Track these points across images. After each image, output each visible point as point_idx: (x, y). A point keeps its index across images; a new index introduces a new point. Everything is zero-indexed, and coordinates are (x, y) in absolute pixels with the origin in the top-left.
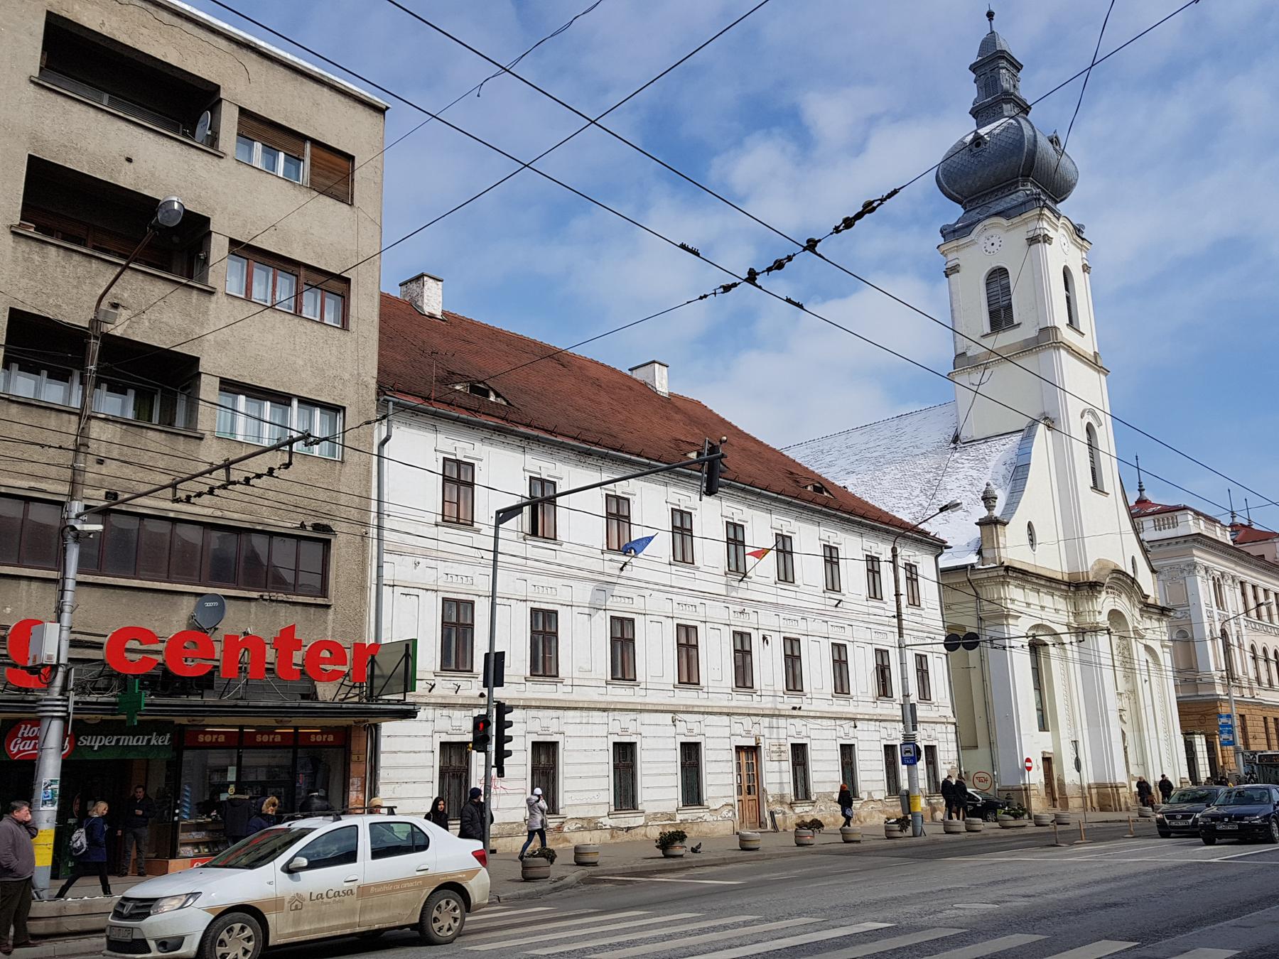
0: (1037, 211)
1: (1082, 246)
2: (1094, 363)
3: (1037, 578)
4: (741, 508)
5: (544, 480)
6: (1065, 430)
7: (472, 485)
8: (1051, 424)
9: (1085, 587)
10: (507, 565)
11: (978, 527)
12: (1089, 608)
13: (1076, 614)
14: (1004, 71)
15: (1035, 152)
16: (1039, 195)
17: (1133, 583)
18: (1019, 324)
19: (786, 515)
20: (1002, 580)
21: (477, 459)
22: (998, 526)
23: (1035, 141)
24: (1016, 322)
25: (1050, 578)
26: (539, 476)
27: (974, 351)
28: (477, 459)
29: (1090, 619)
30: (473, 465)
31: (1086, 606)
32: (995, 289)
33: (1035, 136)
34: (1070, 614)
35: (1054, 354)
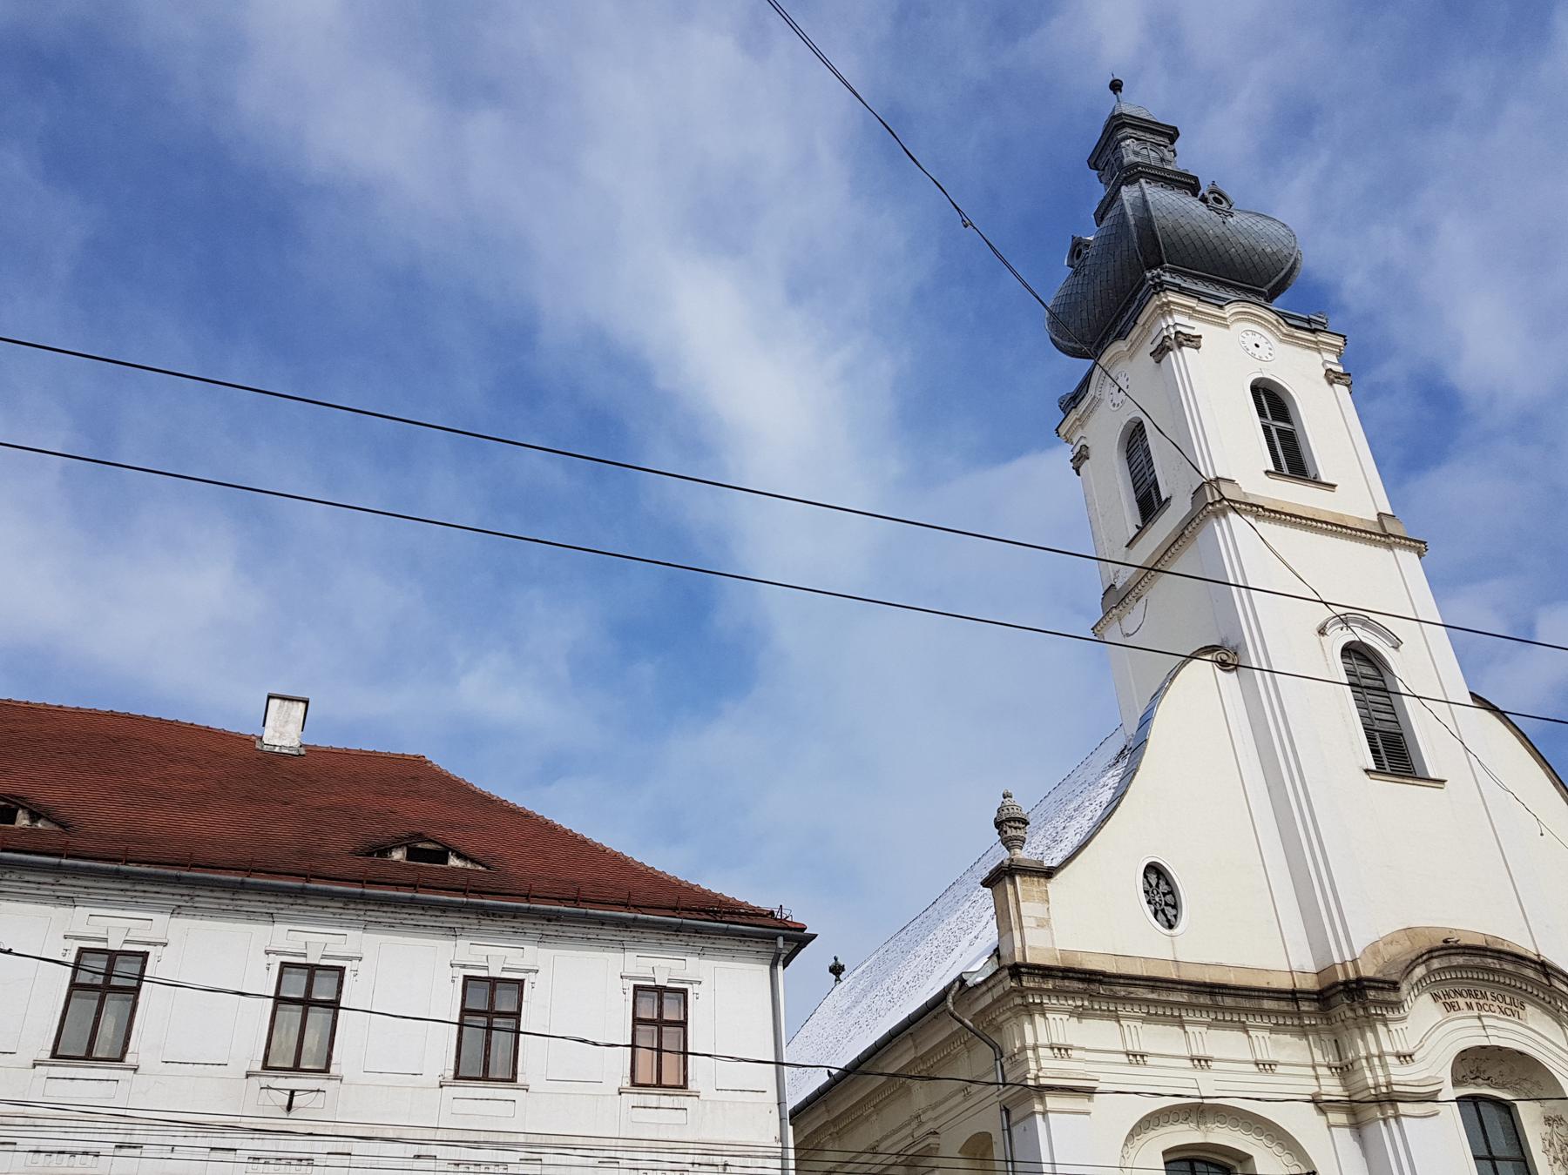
0: (1156, 301)
1: (1316, 343)
2: (1380, 535)
3: (1153, 989)
4: (684, 958)
5: (494, 979)
6: (1259, 662)
7: (334, 1005)
8: (1227, 657)
9: (1339, 997)
10: (92, 1130)
11: (988, 891)
12: (1367, 1047)
13: (1344, 1070)
14: (1128, 142)
15: (1150, 219)
16: (1159, 276)
17: (1547, 976)
18: (1167, 499)
19: (138, 905)
20: (1018, 1001)
21: (691, 983)
22: (1018, 879)
23: (1145, 201)
24: (1163, 499)
25: (1205, 985)
26: (652, 984)
27: (1125, 576)
28: (691, 983)
29: (1375, 1077)
30: (685, 991)
31: (1364, 1045)
32: (1139, 461)
33: (1144, 195)
34: (1323, 1071)
35: (1219, 528)
